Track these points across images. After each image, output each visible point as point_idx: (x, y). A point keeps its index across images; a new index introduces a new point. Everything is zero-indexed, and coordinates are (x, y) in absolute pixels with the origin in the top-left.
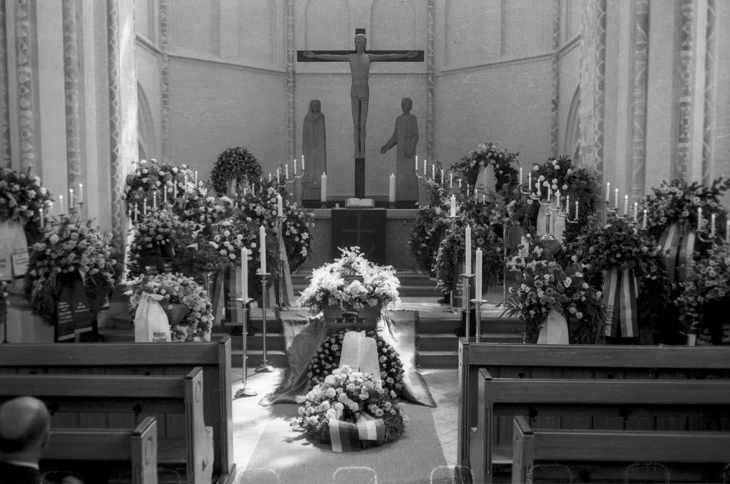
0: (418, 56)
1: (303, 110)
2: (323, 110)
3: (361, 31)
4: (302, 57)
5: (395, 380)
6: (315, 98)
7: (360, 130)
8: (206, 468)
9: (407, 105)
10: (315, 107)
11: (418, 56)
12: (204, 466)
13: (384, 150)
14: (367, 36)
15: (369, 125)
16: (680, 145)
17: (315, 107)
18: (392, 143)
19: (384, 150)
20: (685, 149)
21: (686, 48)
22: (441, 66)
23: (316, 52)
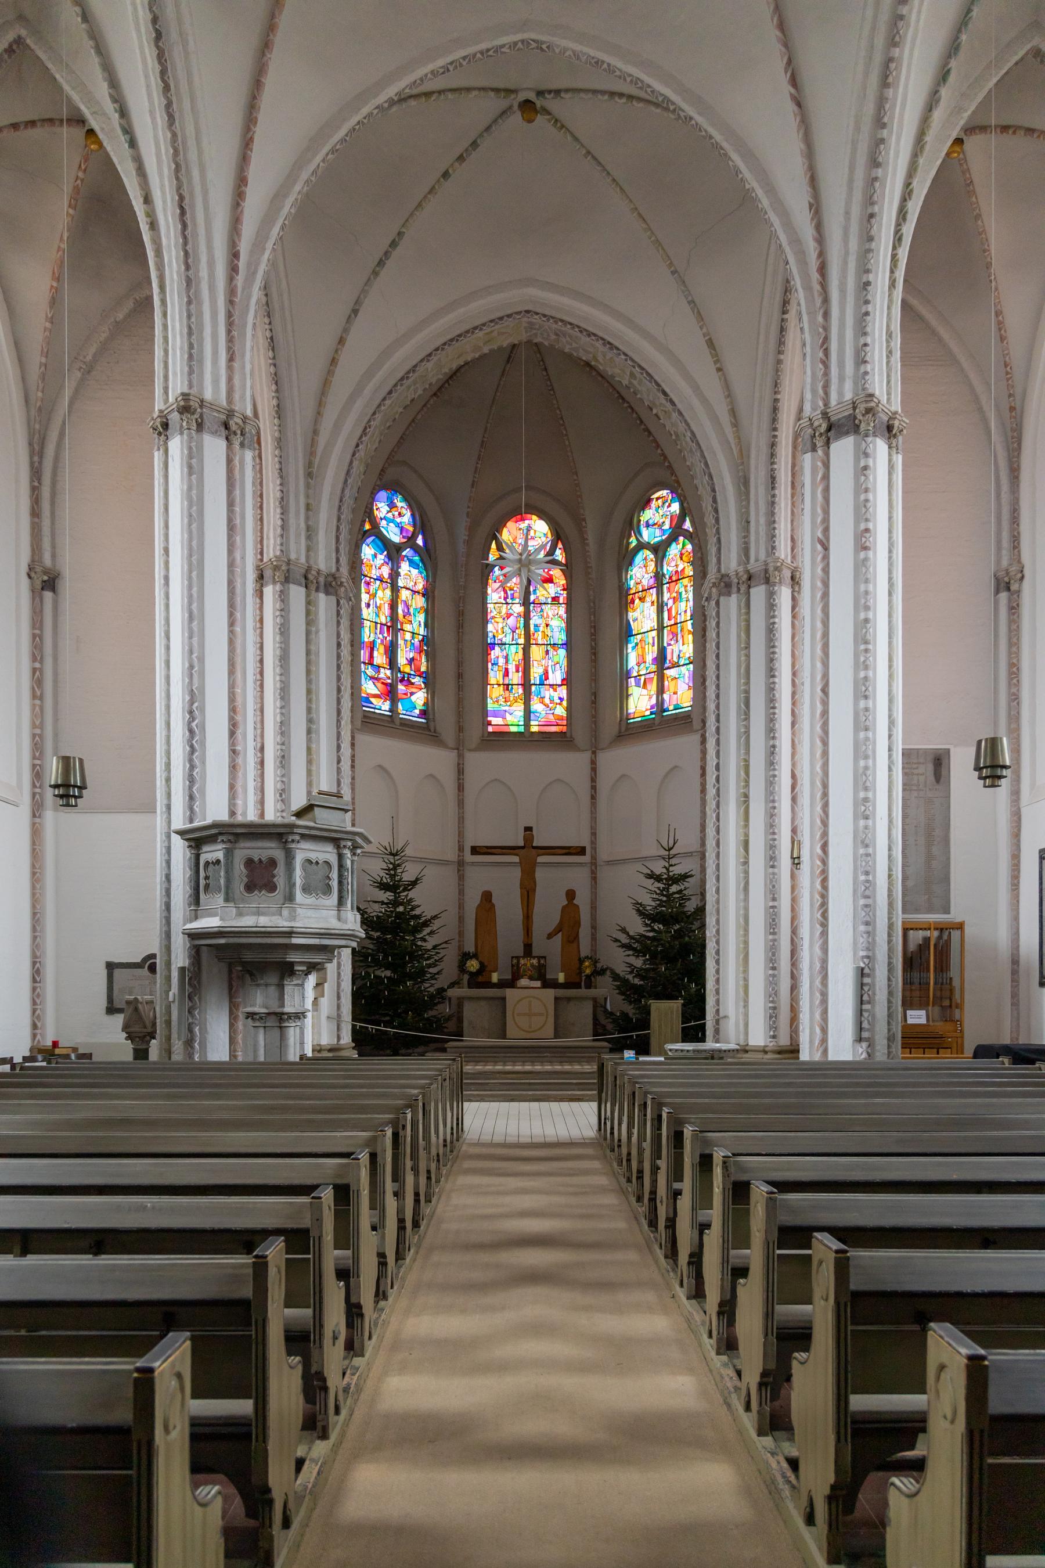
0: (581, 851)
1: (473, 900)
2: (494, 901)
3: (528, 829)
4: (475, 850)
5: (672, 538)
6: (486, 889)
7: (528, 918)
8: (337, 1342)
9: (571, 895)
10: (487, 896)
11: (581, 851)
12: (335, 1338)
13: (550, 936)
14: (534, 832)
15: (536, 918)
16: (771, 680)
17: (487, 896)
18: (558, 929)
19: (550, 936)
20: (774, 714)
21: (774, 647)
22: (603, 855)
23: (487, 847)
